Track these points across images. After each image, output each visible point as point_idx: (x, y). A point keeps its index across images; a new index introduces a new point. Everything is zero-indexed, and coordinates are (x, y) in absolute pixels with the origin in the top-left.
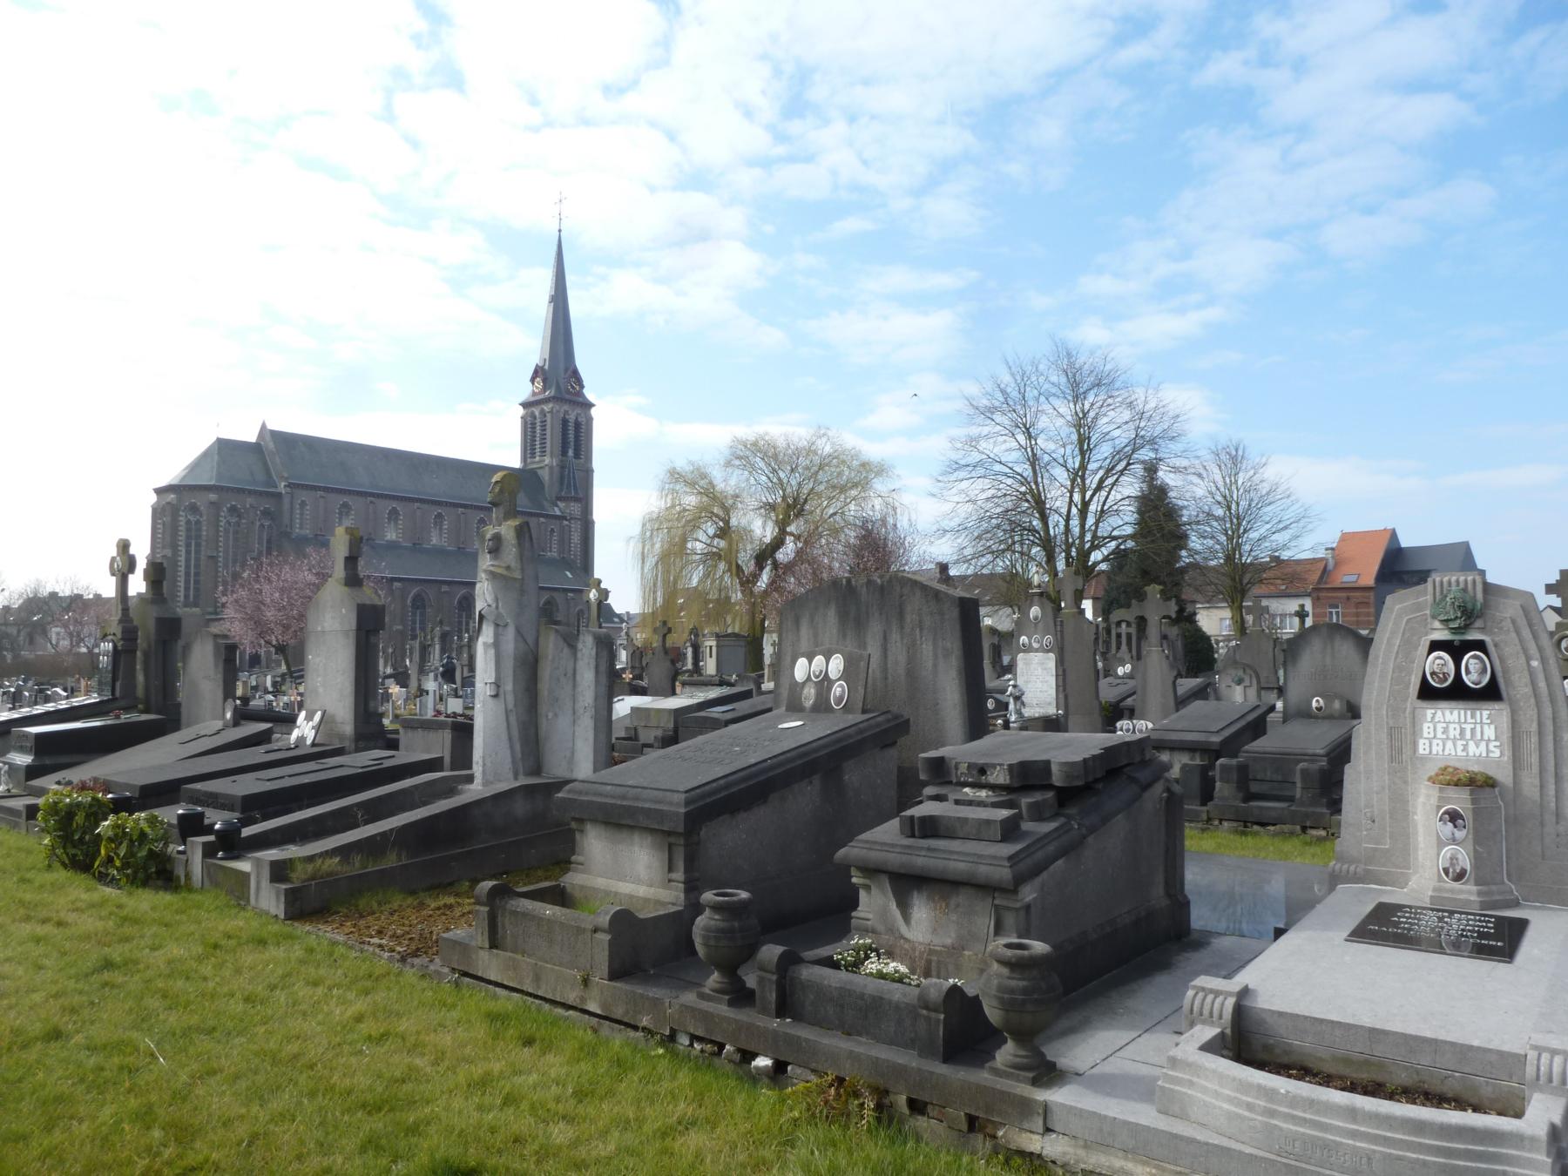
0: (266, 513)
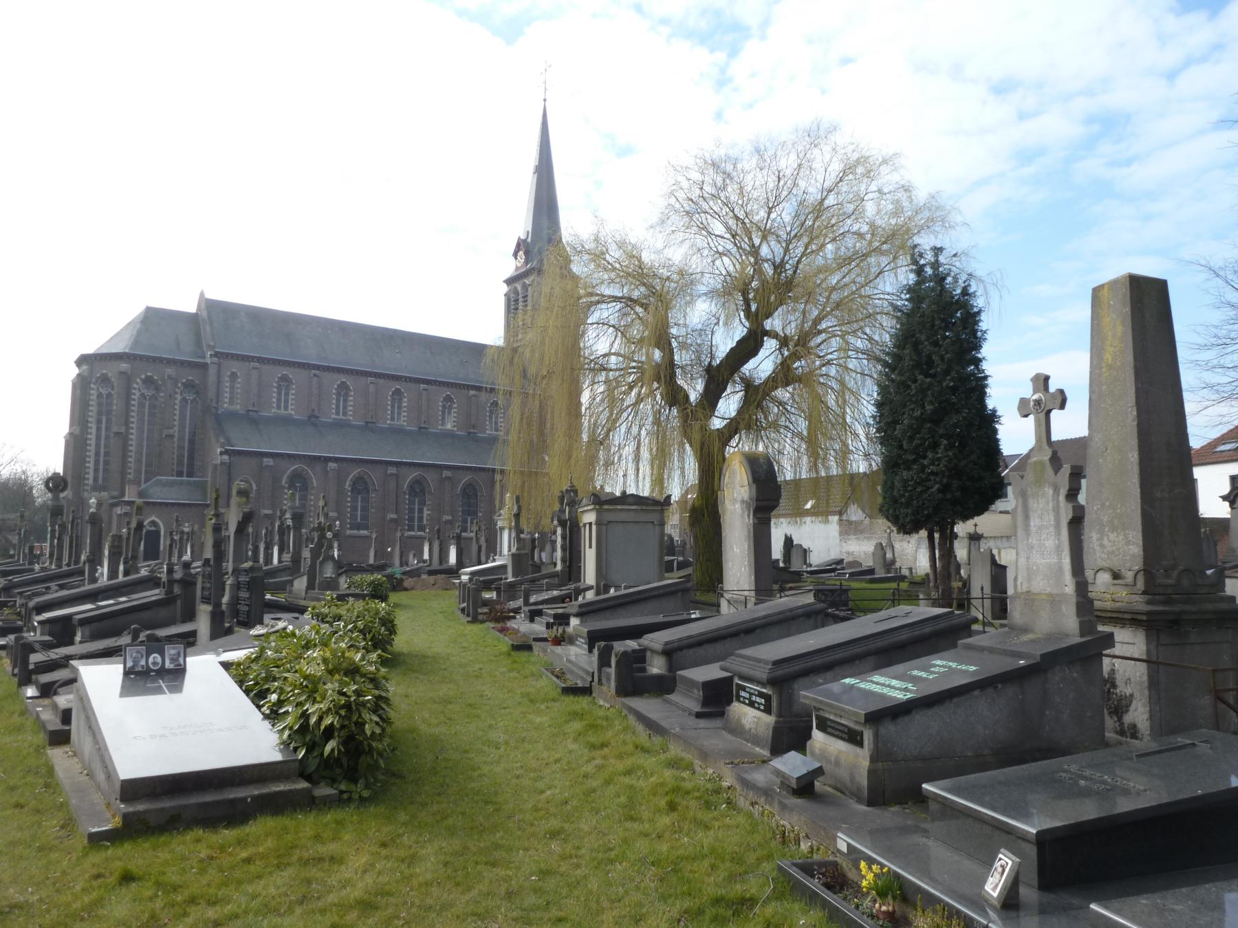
0: (189, 386)
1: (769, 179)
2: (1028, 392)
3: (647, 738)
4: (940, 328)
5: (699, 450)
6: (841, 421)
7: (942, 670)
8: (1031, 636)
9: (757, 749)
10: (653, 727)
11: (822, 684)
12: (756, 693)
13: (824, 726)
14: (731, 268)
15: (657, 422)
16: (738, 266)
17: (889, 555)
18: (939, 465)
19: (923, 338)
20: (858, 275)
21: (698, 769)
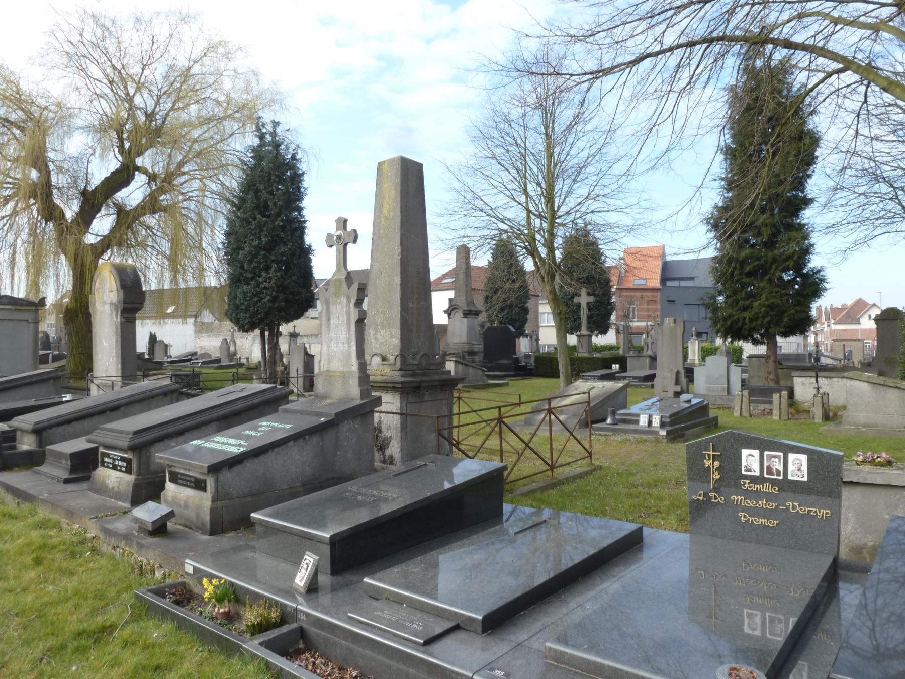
1: (144, 41)
2: (333, 229)
3: (16, 506)
4: (274, 181)
5: (73, 260)
6: (197, 245)
7: (267, 429)
8: (329, 401)
9: (120, 503)
10: (20, 495)
11: (174, 446)
12: (119, 458)
13: (175, 479)
14: (108, 110)
15: (33, 233)
16: (114, 109)
17: (232, 349)
18: (270, 282)
19: (262, 187)
20: (215, 134)
21: (65, 526)
